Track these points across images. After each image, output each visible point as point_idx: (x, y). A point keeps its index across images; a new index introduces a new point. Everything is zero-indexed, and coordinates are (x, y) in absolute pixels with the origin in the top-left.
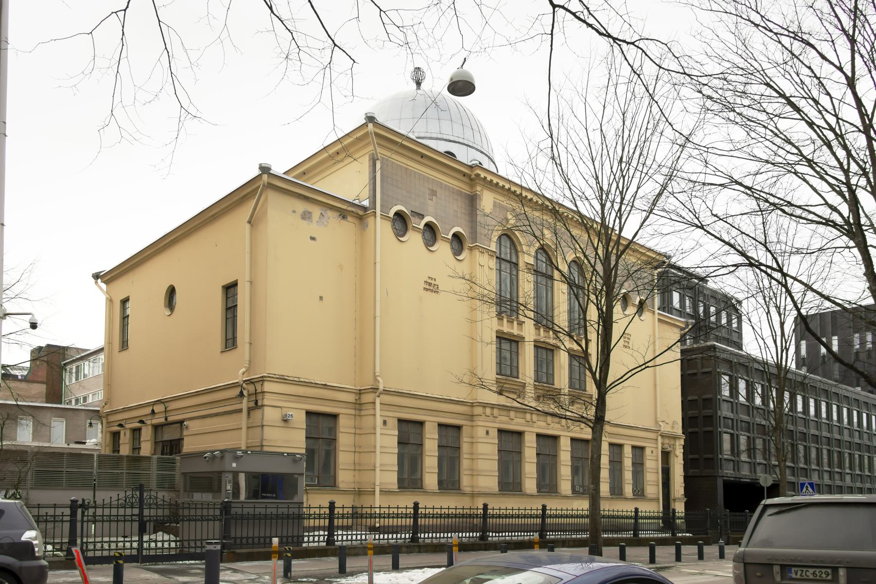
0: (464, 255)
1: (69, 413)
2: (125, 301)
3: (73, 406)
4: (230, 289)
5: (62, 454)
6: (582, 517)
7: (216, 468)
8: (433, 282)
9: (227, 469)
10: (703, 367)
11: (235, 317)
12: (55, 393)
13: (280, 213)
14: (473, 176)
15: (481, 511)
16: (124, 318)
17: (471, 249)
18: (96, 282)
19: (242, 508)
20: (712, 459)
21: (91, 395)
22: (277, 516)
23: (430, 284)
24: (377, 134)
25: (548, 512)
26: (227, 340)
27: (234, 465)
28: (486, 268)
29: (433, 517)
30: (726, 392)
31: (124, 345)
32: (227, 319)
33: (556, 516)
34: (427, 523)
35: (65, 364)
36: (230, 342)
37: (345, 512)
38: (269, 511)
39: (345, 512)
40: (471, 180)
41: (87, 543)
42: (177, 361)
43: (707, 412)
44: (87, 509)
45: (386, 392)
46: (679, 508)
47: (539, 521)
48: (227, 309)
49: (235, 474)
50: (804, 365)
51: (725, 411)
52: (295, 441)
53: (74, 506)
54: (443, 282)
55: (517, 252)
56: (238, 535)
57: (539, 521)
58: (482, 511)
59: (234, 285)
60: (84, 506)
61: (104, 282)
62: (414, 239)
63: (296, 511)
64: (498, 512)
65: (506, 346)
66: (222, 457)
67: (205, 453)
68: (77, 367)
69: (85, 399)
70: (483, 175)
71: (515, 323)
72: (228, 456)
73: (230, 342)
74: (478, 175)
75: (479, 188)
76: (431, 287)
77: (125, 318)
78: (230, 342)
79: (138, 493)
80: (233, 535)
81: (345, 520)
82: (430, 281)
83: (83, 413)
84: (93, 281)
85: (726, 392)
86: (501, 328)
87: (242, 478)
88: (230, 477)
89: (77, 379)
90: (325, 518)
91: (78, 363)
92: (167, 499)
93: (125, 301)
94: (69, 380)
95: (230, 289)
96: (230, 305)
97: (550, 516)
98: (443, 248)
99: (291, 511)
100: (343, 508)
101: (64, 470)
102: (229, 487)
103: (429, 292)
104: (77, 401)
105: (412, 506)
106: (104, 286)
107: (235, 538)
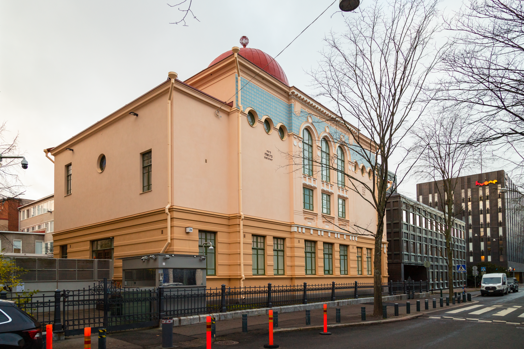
0: (286, 137)
1: (24, 236)
2: (68, 166)
3: (25, 232)
4: (146, 155)
5: (35, 259)
6: (327, 289)
7: (151, 265)
8: (269, 154)
9: (160, 267)
10: (393, 207)
11: (149, 172)
12: (14, 224)
13: (182, 107)
14: (290, 93)
15: (267, 289)
16: (68, 176)
17: (289, 136)
18: (47, 156)
19: (170, 291)
20: (399, 254)
21: (37, 227)
22: (192, 296)
23: (268, 155)
24: (241, 64)
25: (273, 288)
26: (143, 187)
27: (164, 264)
28: (297, 147)
29: (278, 292)
30: (404, 220)
31: (68, 192)
32: (143, 174)
33: (312, 290)
34: (254, 297)
35: (20, 209)
36: (146, 188)
37: (212, 292)
38: (187, 293)
39: (218, 292)
40: (289, 95)
41: (68, 321)
42: (114, 198)
43: (397, 230)
44: (68, 297)
45: (246, 218)
46: (385, 281)
47: (331, 291)
48: (144, 168)
49: (165, 269)
50: (436, 205)
51: (404, 230)
52: (192, 247)
53: (57, 295)
54: (274, 153)
55: (312, 140)
56: (168, 309)
57: (331, 291)
58: (267, 288)
59: (149, 152)
60: (65, 294)
61: (53, 155)
62: (260, 127)
63: (203, 292)
64: (281, 288)
65: (307, 192)
66: (155, 260)
67: (142, 257)
68: (28, 211)
69: (33, 228)
70: (296, 93)
71: (312, 179)
72: (160, 258)
73: (147, 187)
74: (293, 93)
75: (293, 101)
76: (268, 156)
77: (68, 176)
78: (147, 187)
79: (103, 285)
80: (165, 310)
81: (218, 297)
82: (268, 153)
83: (33, 237)
84: (45, 154)
85: (404, 220)
86: (305, 182)
87: (171, 272)
88: (161, 272)
89: (28, 216)
90: (219, 296)
91: (27, 208)
92: (92, 287)
93: (68, 166)
94: (23, 216)
95: (146, 155)
96: (146, 165)
97: (309, 290)
98: (275, 134)
99: (200, 292)
100: (211, 290)
101: (37, 269)
102: (161, 279)
103: (267, 160)
104: (28, 230)
105: (221, 287)
106: (53, 158)
107: (167, 311)
